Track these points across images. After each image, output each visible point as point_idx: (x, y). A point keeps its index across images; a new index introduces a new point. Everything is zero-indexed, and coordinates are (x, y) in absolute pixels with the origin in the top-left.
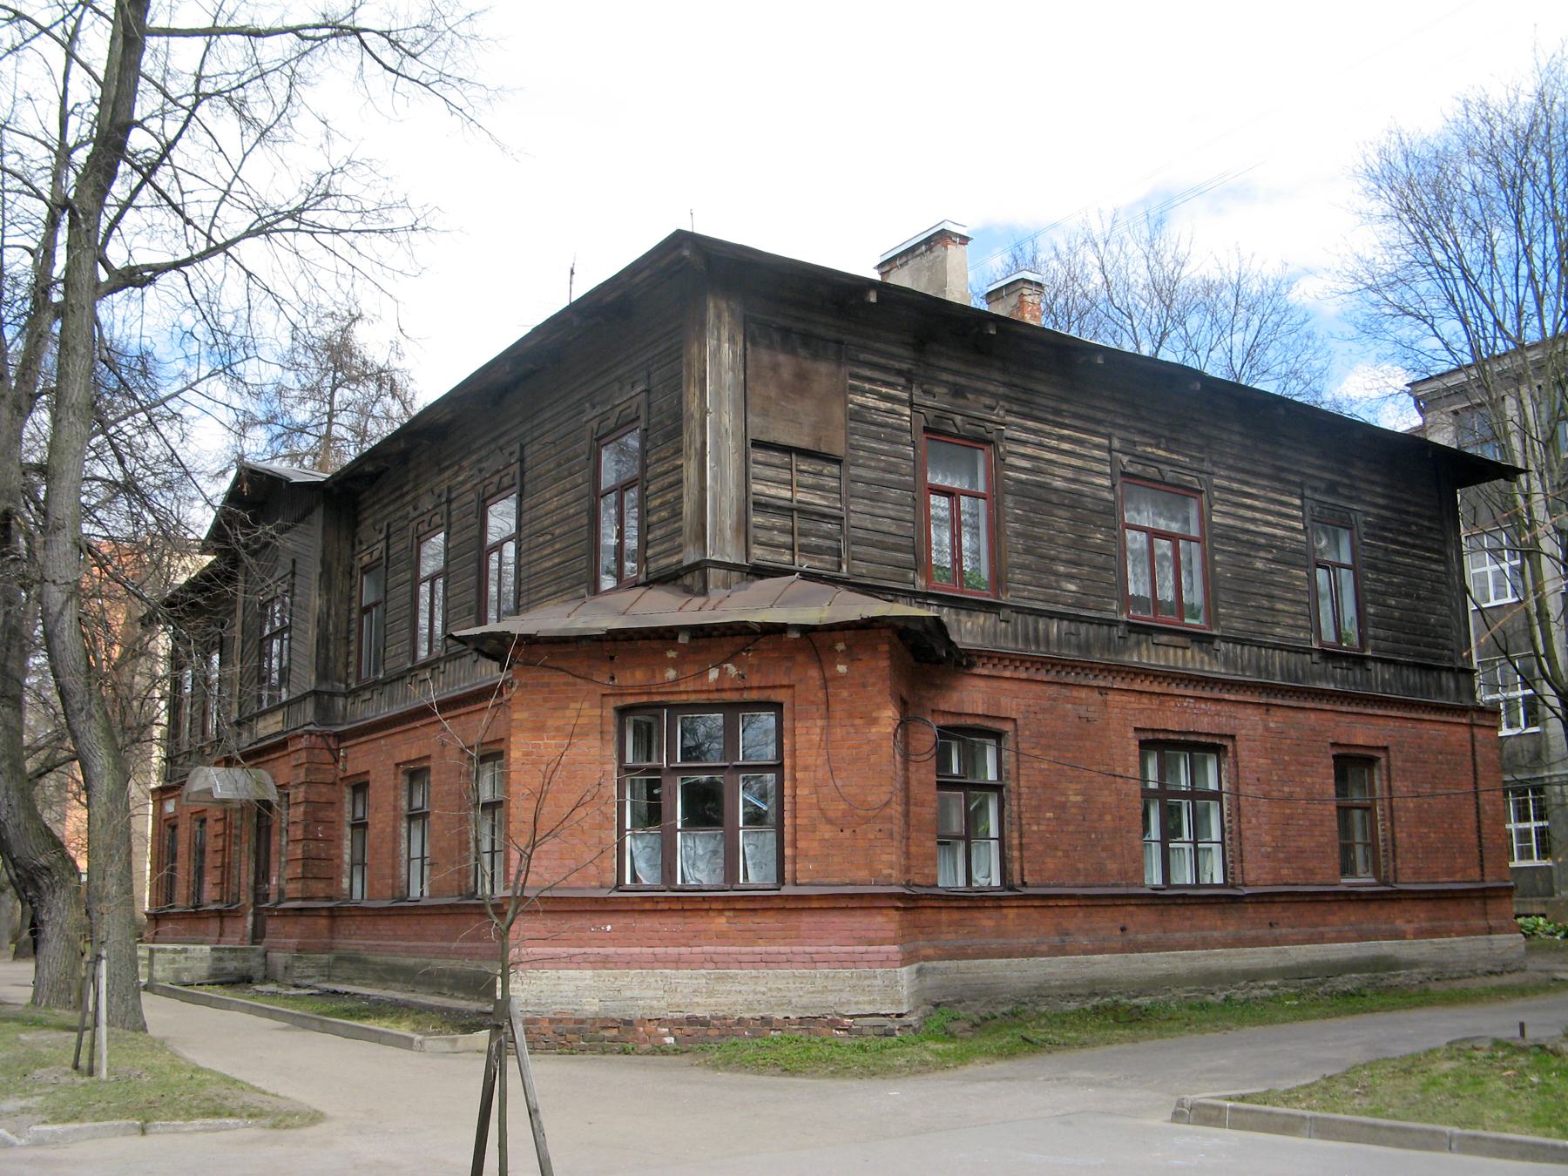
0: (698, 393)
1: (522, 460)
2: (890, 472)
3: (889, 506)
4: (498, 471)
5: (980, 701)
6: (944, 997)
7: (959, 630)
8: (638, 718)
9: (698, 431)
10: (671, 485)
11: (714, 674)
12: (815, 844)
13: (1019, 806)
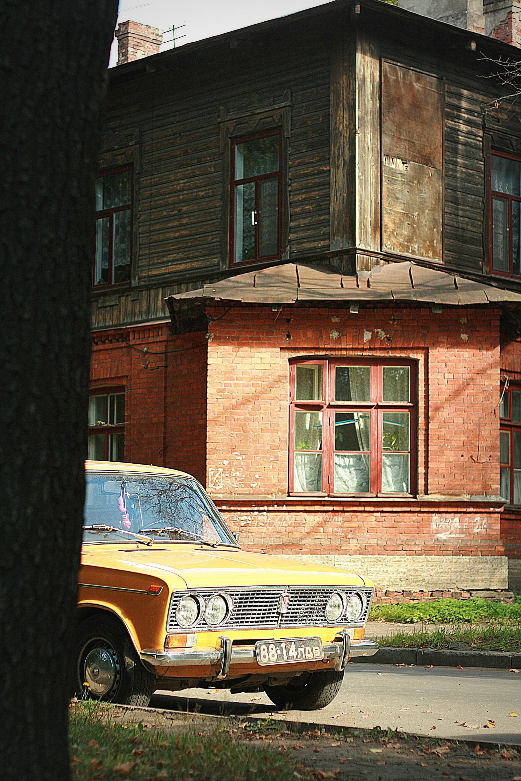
0: (346, 116)
2: (469, 182)
3: (467, 208)
4: (113, 150)
8: (298, 366)
9: (347, 147)
10: (322, 184)
11: (367, 336)
12: (443, 465)
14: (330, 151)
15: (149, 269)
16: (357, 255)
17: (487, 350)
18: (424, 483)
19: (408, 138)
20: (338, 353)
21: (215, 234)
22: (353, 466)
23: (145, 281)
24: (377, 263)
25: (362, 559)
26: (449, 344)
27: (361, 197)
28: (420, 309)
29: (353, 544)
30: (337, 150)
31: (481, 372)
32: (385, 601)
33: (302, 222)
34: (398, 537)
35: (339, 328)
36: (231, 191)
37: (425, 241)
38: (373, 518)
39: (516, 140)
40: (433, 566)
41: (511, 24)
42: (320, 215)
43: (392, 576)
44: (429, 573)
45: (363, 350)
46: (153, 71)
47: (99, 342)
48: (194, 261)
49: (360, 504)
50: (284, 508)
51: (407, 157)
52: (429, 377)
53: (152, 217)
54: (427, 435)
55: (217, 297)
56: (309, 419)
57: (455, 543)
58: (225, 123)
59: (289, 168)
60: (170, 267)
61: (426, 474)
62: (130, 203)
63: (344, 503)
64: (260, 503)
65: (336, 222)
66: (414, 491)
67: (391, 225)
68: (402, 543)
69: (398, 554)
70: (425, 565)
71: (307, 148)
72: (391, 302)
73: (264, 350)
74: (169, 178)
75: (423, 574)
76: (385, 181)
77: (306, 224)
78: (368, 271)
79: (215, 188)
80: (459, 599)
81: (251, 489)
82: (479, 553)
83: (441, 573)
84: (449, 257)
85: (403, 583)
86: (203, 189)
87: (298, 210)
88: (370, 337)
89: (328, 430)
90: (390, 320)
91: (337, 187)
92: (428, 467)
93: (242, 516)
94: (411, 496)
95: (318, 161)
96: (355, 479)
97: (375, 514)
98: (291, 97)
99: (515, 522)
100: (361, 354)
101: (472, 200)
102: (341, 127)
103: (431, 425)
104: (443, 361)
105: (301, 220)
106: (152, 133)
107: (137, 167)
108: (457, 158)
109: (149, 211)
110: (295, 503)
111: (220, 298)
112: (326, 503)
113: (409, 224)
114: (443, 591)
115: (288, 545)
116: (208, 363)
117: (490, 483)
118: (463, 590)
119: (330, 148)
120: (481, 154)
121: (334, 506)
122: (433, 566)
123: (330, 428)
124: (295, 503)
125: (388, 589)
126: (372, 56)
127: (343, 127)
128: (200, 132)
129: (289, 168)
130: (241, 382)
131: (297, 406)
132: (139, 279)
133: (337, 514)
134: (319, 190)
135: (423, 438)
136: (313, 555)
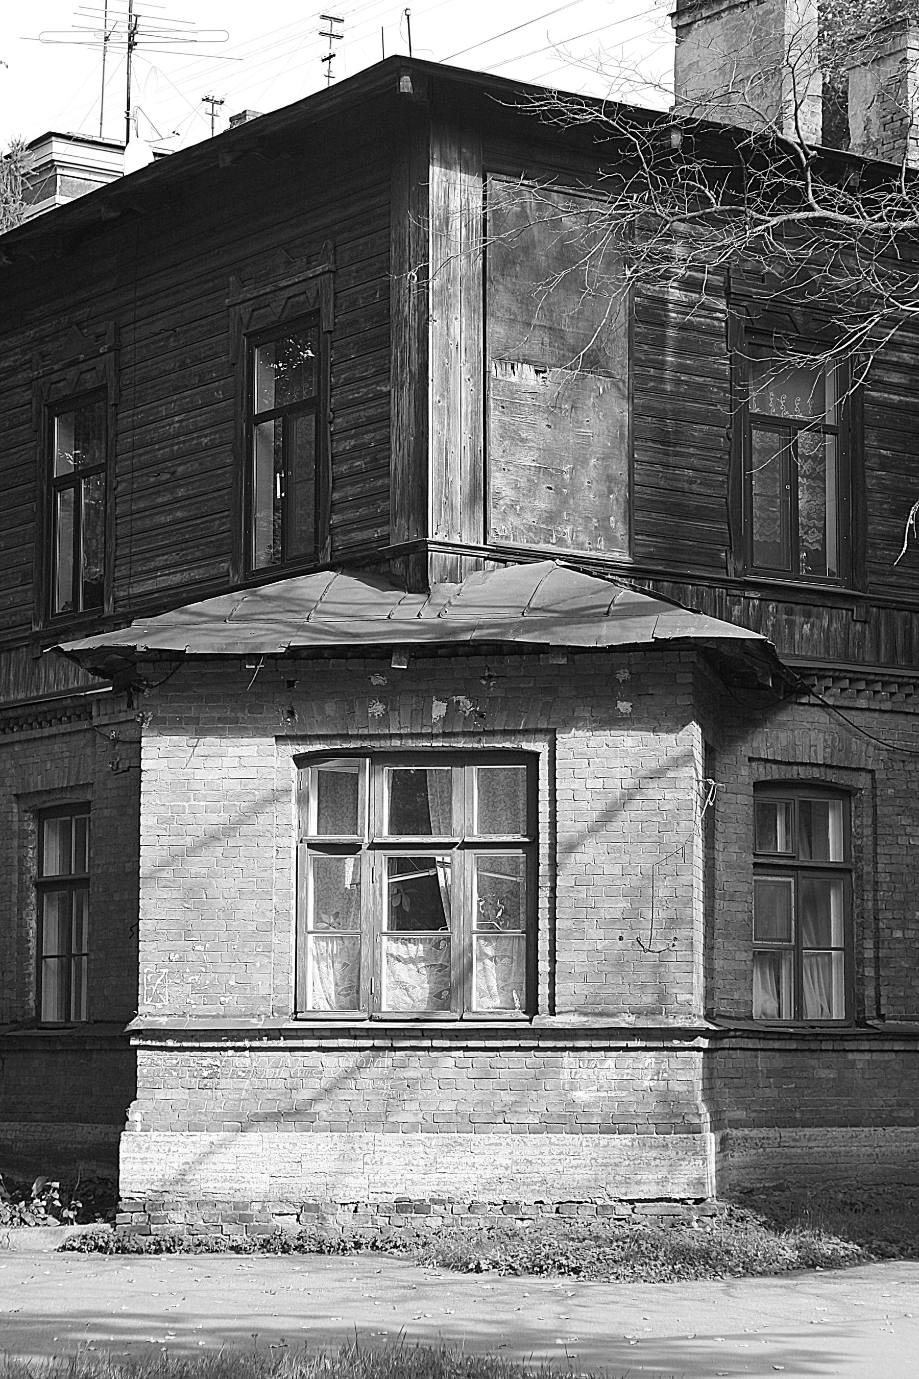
1: (116, 349)
4: (76, 362)
5: (822, 744)
6: (760, 1180)
7: (792, 637)
9: (415, 346)
10: (371, 421)
11: (439, 710)
12: (583, 957)
13: (876, 900)
14: (390, 355)
15: (130, 583)
16: (430, 553)
17: (669, 731)
18: (548, 992)
19: (548, 324)
20: (385, 744)
21: (223, 517)
22: (424, 960)
23: (124, 606)
24: (477, 567)
25: (426, 1141)
26: (595, 721)
27: (439, 442)
28: (539, 655)
29: (408, 1114)
30: (401, 352)
31: (656, 775)
32: (466, 1223)
33: (351, 491)
34: (498, 1097)
35: (383, 695)
36: (247, 435)
37: (588, 519)
38: (448, 1061)
39: (804, 314)
40: (561, 1153)
41: (906, 82)
42: (376, 478)
43: (482, 1172)
44: (554, 1168)
45: (432, 736)
46: (113, 215)
47: (53, 721)
48: (194, 568)
49: (424, 1034)
50: (282, 1043)
51: (548, 359)
52: (557, 787)
53: (135, 486)
54: (553, 898)
55: (141, 645)
56: (352, 869)
57: (606, 1109)
58: (237, 307)
59: (331, 390)
60: (159, 579)
61: (552, 974)
62: (103, 461)
63: (392, 1033)
64: (235, 1033)
65: (398, 492)
66: (532, 1008)
67: (508, 493)
68: (504, 1109)
69: (495, 1130)
70: (546, 1152)
71: (358, 351)
72: (462, 645)
73: (245, 741)
74: (158, 412)
75: (542, 1169)
76: (495, 409)
77: (356, 495)
78: (456, 583)
79: (224, 430)
80: (610, 1219)
81: (222, 1007)
82: (653, 1128)
83: (576, 1167)
84: (649, 546)
85: (505, 1186)
86: (208, 431)
87: (344, 468)
88: (443, 713)
89: (371, 892)
90: (483, 678)
91: (400, 424)
92: (556, 961)
93: (205, 1058)
94: (527, 1017)
95: (374, 375)
96: (426, 985)
97: (454, 1054)
98: (335, 254)
99: (799, 1054)
100: (429, 744)
101: (701, 434)
102: (407, 309)
103: (561, 880)
104: (582, 755)
105: (349, 488)
106: (135, 329)
107: (112, 393)
108: (664, 355)
109: (129, 476)
110: (300, 1034)
111: (146, 648)
112: (358, 1033)
113: (550, 488)
114: (582, 1202)
115: (288, 1114)
116: (143, 768)
117: (675, 991)
118: (621, 1201)
119: (391, 350)
120: (724, 345)
121: (373, 1039)
122: (561, 1153)
123: (374, 887)
124: (300, 1034)
125: (476, 1198)
126: (467, 169)
127: (408, 309)
128: (202, 326)
129: (331, 390)
130: (202, 803)
131: (310, 846)
132: (115, 602)
133: (381, 1054)
134: (374, 431)
135: (548, 906)
136: (334, 1134)
